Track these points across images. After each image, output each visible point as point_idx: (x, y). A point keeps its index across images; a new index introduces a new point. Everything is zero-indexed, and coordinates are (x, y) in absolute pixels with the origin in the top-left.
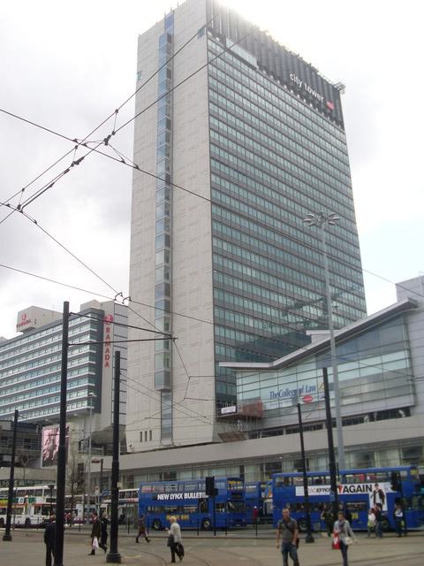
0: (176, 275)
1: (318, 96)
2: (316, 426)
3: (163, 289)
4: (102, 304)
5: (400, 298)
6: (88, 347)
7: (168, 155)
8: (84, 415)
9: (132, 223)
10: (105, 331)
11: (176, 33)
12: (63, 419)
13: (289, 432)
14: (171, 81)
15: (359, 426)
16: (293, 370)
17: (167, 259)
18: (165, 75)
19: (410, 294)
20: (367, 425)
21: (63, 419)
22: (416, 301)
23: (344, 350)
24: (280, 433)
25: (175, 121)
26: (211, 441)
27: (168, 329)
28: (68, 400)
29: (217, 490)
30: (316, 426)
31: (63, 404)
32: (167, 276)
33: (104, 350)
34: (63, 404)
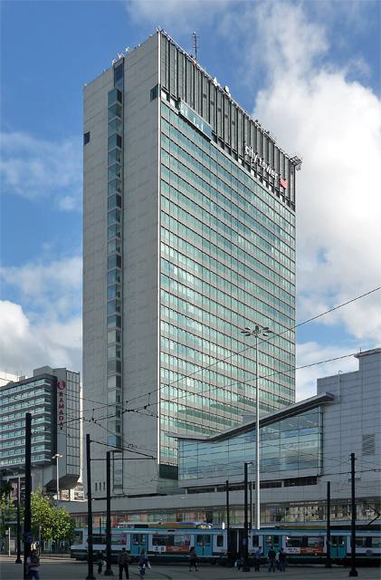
0: (127, 354)
1: (269, 170)
2: (236, 487)
3: (115, 365)
4: (54, 370)
5: (319, 393)
6: (43, 381)
7: (118, 235)
8: (43, 466)
9: (84, 258)
10: (58, 395)
11: (126, 90)
12: (28, 467)
13: (219, 490)
14: (120, 224)
15: (276, 489)
16: (226, 442)
17: (118, 339)
18: (115, 143)
19: (328, 389)
20: (283, 489)
21: (28, 467)
22: (333, 395)
23: (269, 429)
24: (213, 490)
25: (125, 318)
26: (155, 492)
27: (119, 432)
28: (32, 443)
29: (318, 73)
30: (236, 487)
31: (28, 455)
32: (118, 354)
33: (58, 400)
34: (28, 455)
